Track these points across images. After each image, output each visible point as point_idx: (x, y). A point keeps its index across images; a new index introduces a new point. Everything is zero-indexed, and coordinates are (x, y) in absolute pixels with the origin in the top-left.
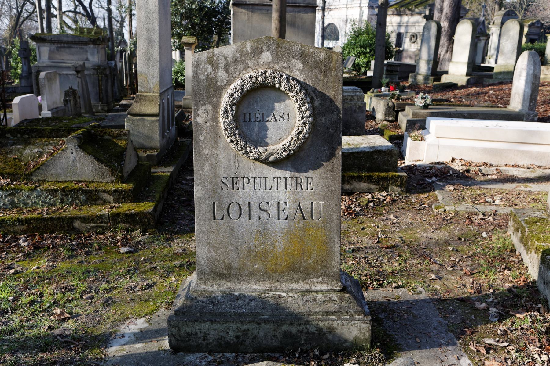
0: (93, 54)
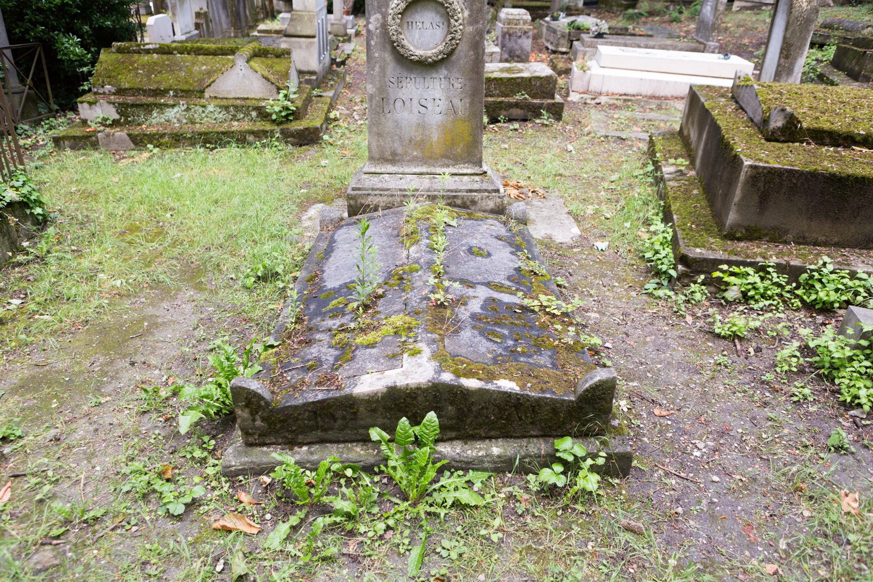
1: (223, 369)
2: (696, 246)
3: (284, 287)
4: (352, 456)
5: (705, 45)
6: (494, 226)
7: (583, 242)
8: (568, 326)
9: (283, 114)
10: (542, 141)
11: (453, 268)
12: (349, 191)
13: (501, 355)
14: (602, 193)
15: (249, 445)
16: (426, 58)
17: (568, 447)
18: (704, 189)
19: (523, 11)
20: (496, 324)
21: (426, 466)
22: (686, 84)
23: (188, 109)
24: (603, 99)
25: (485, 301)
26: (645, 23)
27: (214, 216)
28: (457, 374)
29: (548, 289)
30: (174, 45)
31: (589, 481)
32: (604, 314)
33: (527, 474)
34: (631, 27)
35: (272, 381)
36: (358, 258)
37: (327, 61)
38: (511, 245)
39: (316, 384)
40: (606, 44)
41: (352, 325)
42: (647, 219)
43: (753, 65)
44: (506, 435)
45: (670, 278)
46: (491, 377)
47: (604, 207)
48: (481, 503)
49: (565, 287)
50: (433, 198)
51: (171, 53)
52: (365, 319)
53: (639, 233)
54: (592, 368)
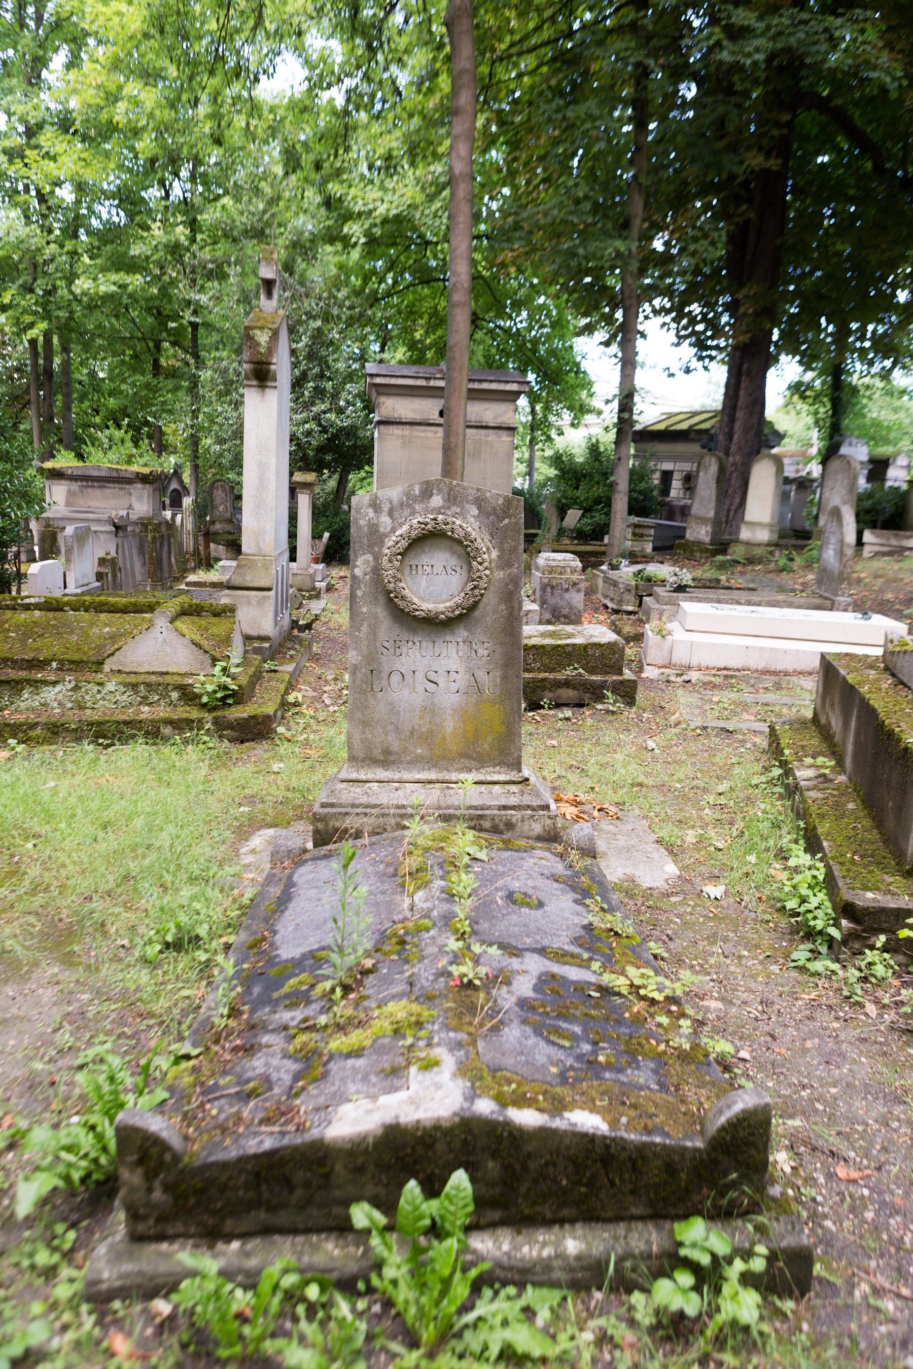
0: (140, 498)
1: (101, 1097)
2: (866, 888)
3: (209, 960)
4: (319, 1259)
5: (833, 602)
6: (543, 860)
7: (685, 885)
8: (678, 1018)
9: (219, 695)
10: (609, 735)
11: (484, 926)
12: (317, 809)
13: (572, 1068)
14: (707, 811)
15: (137, 1238)
16: (437, 614)
17: (699, 1236)
18: (863, 801)
19: (570, 556)
20: (560, 1016)
21: (452, 1275)
22: (813, 653)
23: (76, 688)
24: (694, 676)
25: (539, 978)
26: (742, 573)
27: (102, 847)
28: (502, 1101)
29: (639, 958)
30: (66, 599)
31: (743, 1305)
32: (731, 1002)
33: (629, 1292)
34: (723, 578)
35: (185, 1115)
36: (330, 910)
37: (286, 622)
38: (574, 889)
39: (261, 1122)
40: (691, 599)
41: (323, 1020)
42: (781, 850)
43: (906, 627)
44: (588, 1214)
45: (831, 941)
46: (558, 1107)
47: (712, 833)
48: (553, 1351)
49: (663, 959)
50: (446, 818)
51: (62, 610)
52: (343, 1009)
53: (772, 872)
54: (725, 1091)
